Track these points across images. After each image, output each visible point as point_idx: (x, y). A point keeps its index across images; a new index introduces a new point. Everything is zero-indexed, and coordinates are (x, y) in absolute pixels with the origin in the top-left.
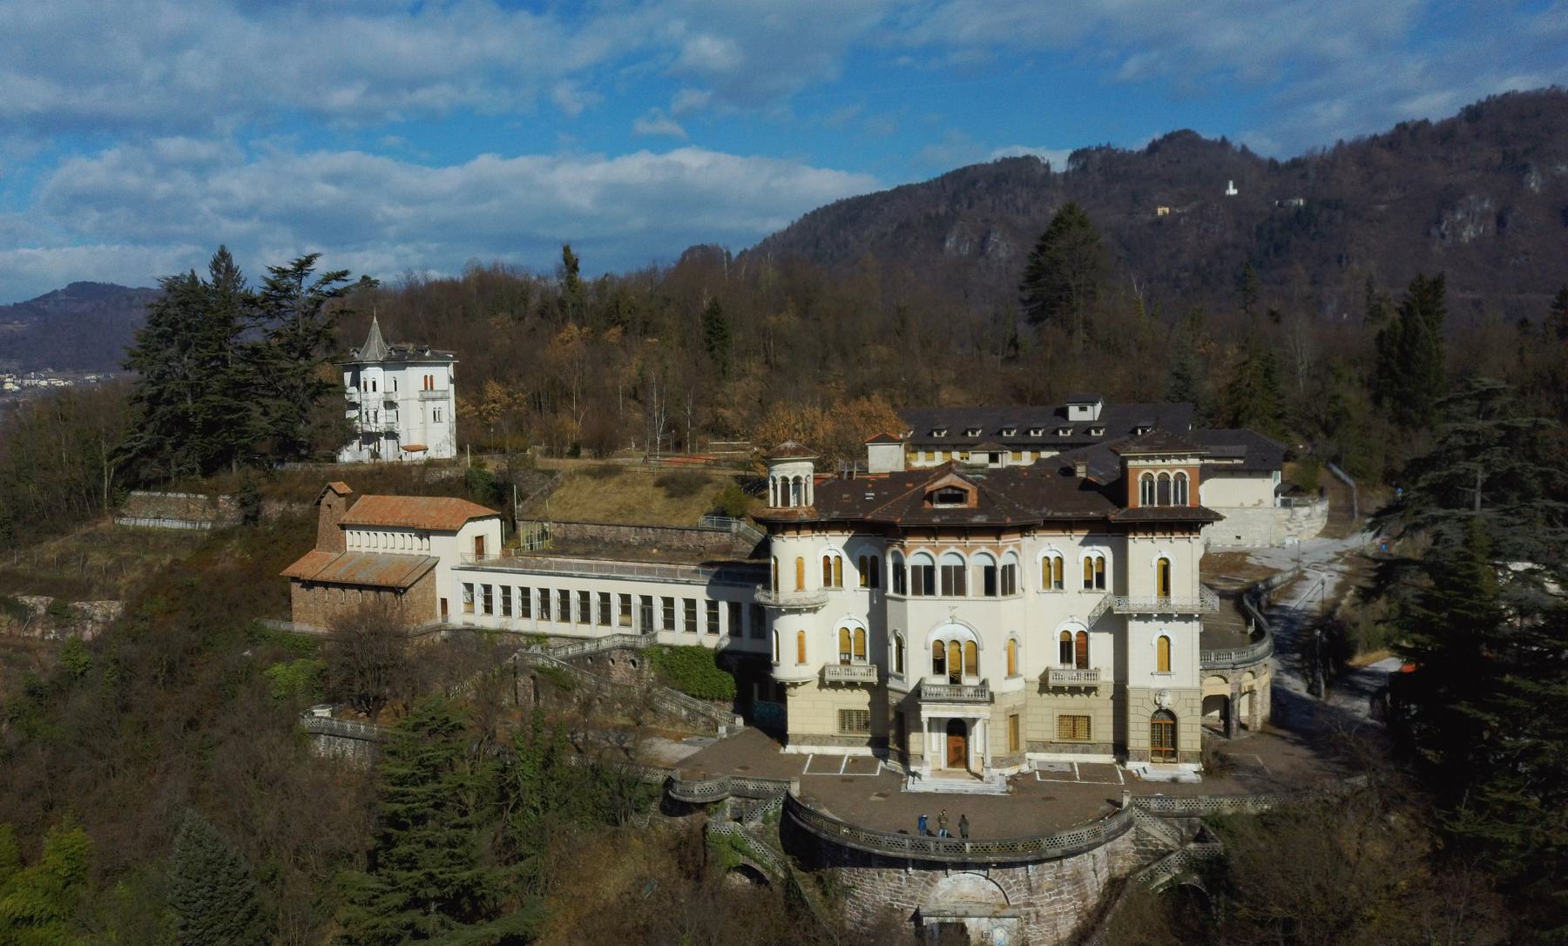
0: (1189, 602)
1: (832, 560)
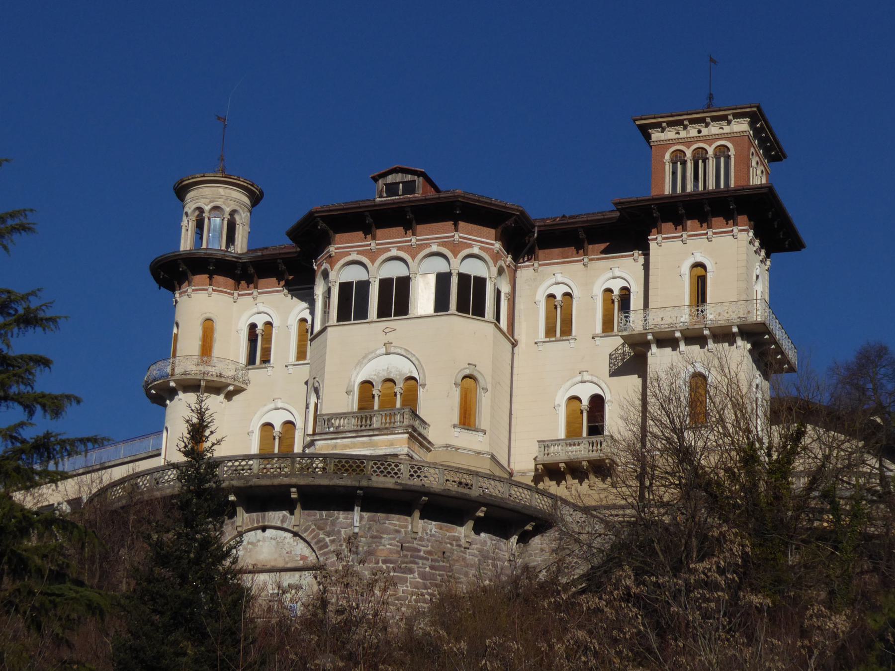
0: (666, 245)
1: (260, 326)
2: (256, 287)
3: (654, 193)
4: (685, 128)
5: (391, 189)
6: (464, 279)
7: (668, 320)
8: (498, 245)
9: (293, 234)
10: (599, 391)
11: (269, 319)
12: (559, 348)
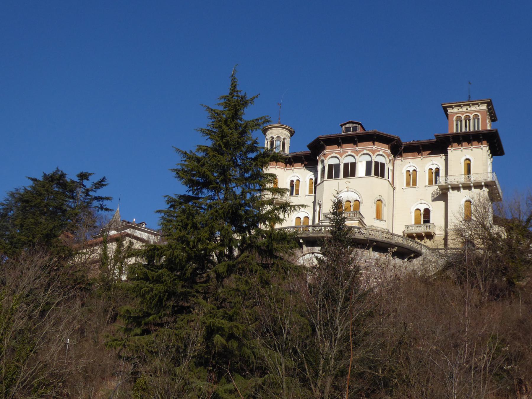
0: (455, 152)
1: (294, 183)
2: (293, 167)
3: (450, 132)
4: (462, 108)
5: (348, 129)
6: (377, 163)
7: (479, 179)
8: (389, 151)
9: (310, 147)
10: (428, 207)
11: (298, 178)
12: (412, 191)
